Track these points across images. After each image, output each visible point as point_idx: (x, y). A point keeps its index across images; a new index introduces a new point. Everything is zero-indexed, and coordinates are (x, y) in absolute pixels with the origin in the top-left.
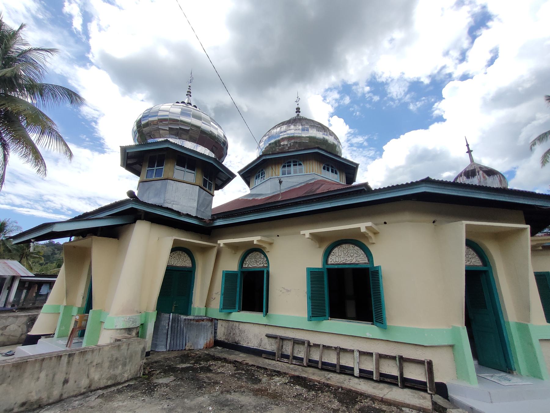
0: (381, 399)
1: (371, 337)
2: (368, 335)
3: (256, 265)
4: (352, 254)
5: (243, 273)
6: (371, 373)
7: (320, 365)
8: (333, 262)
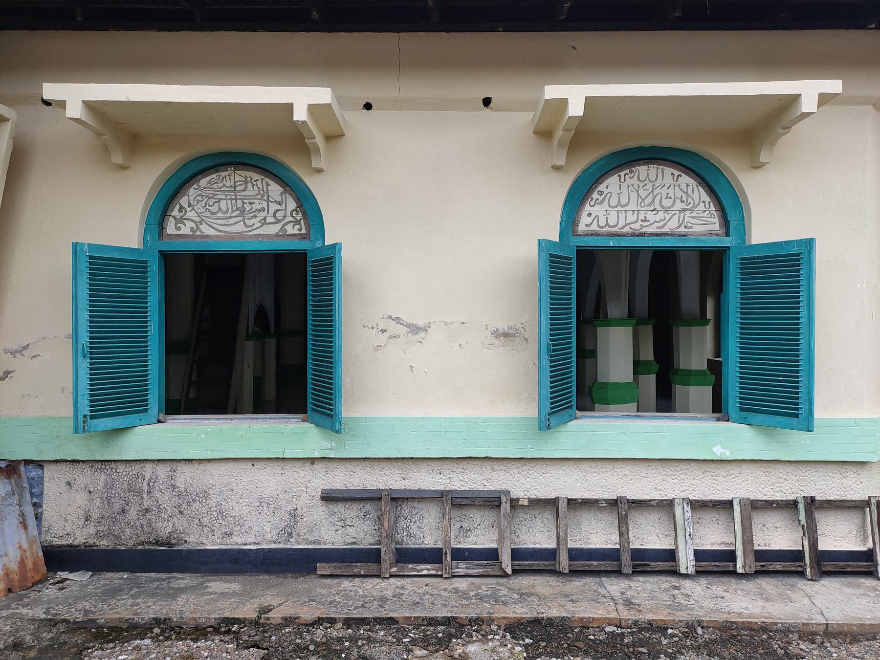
0: (822, 628)
1: (728, 455)
2: (719, 452)
3: (240, 228)
4: (667, 203)
5: (169, 259)
6: (731, 556)
7: (564, 563)
8: (594, 228)
